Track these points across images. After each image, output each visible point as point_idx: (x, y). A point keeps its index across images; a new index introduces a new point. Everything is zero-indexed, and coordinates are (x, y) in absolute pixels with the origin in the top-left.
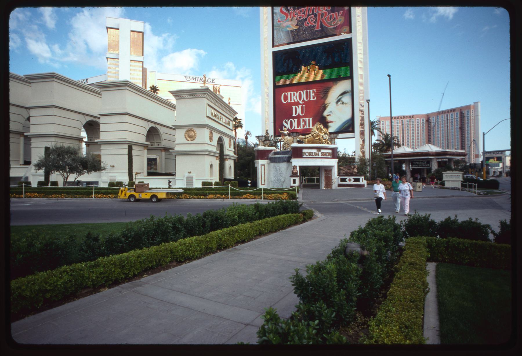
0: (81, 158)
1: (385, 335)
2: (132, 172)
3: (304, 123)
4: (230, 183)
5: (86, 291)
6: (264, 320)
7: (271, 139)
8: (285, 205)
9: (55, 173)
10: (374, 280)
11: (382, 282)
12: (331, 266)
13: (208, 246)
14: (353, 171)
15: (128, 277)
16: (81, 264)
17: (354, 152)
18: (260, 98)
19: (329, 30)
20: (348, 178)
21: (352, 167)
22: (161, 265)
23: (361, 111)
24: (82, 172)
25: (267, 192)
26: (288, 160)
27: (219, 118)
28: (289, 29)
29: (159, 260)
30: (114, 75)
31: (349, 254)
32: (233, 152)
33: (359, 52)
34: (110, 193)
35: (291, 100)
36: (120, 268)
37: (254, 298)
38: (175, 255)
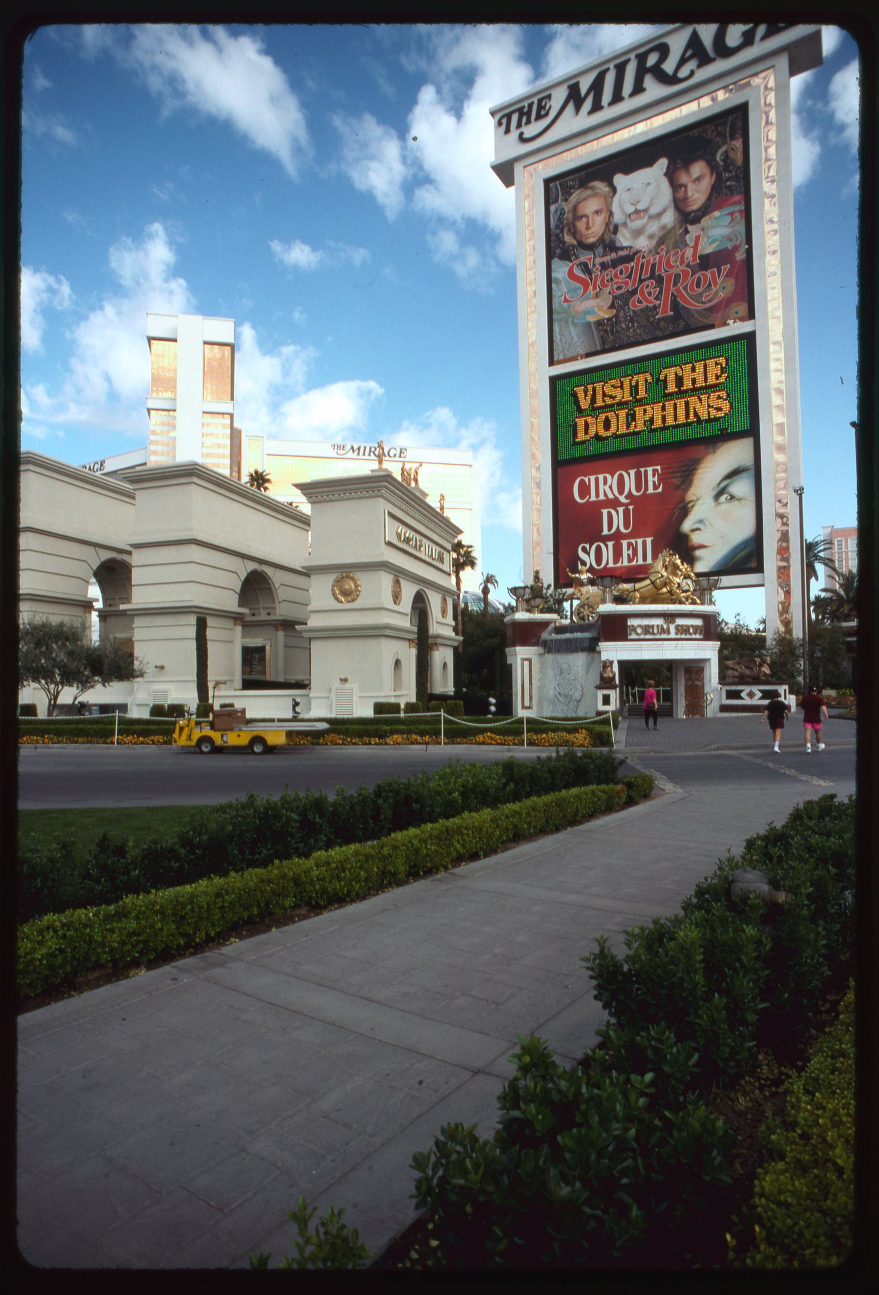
0: (89, 649)
1: (828, 1121)
2: (206, 681)
3: (630, 552)
4: (444, 704)
5: (96, 974)
6: (516, 1067)
7: (548, 594)
8: (579, 762)
9: (29, 685)
10: (806, 968)
11: (829, 973)
12: (689, 934)
13: (385, 868)
14: (760, 672)
15: (193, 944)
16: (85, 911)
17: (764, 622)
18: (520, 492)
19: (696, 315)
20: (746, 689)
21: (758, 660)
22: (271, 914)
23: (781, 516)
24: (89, 683)
25: (536, 726)
26: (591, 648)
27: (416, 545)
28: (591, 319)
29: (267, 904)
30: (165, 448)
31: (738, 899)
32: (452, 628)
33: (773, 365)
34: (154, 733)
35: (597, 495)
36: (173, 922)
37: (496, 1004)
38: (305, 891)
